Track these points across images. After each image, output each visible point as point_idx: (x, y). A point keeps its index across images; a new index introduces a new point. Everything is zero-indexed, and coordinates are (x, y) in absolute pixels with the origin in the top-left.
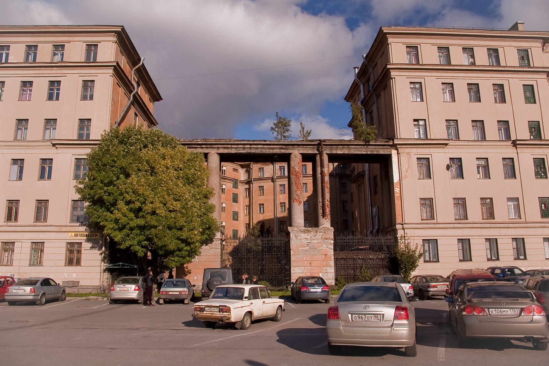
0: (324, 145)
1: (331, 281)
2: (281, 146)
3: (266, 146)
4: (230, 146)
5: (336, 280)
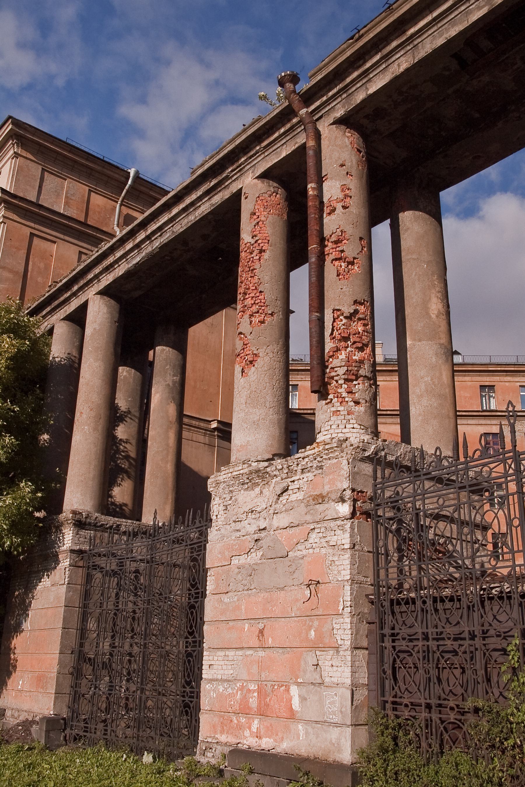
1: (334, 734)
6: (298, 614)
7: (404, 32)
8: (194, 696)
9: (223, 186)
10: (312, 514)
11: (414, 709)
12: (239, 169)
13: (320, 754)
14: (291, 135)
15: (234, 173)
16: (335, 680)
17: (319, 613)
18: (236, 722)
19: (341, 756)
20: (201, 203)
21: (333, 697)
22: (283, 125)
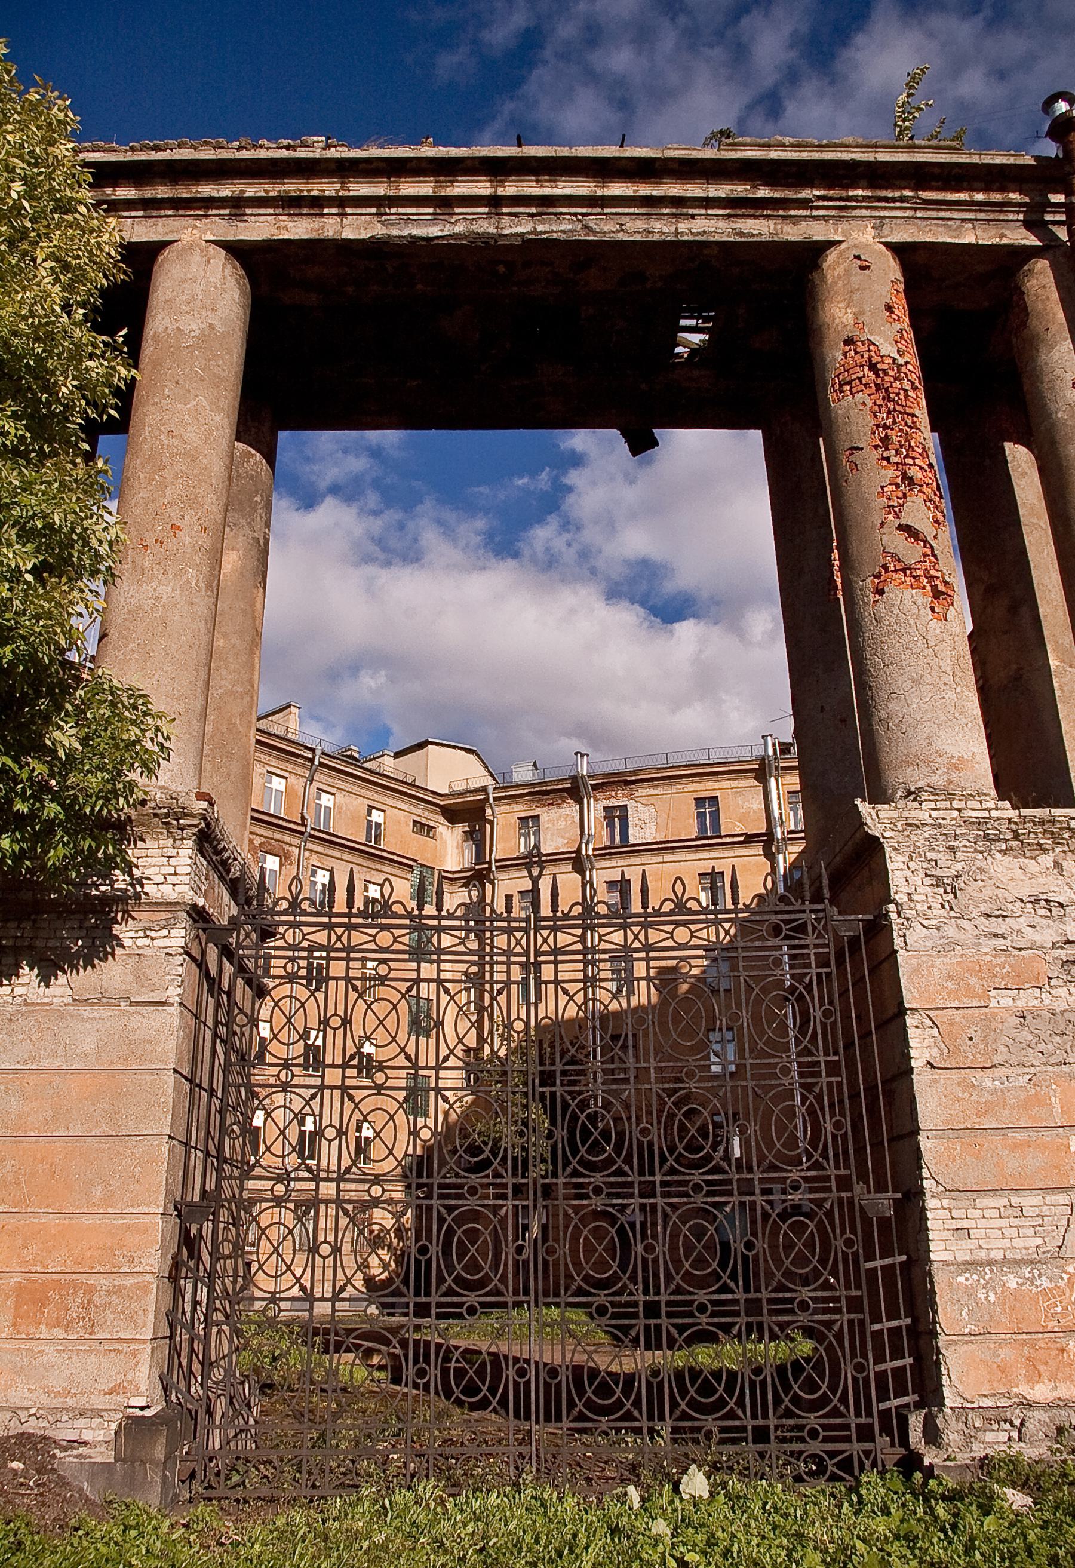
2: (741, 190)
3: (617, 189)
4: (330, 188)
9: (781, 213)
12: (843, 204)
14: (991, 216)
15: (826, 203)
20: (703, 212)
22: (986, 189)
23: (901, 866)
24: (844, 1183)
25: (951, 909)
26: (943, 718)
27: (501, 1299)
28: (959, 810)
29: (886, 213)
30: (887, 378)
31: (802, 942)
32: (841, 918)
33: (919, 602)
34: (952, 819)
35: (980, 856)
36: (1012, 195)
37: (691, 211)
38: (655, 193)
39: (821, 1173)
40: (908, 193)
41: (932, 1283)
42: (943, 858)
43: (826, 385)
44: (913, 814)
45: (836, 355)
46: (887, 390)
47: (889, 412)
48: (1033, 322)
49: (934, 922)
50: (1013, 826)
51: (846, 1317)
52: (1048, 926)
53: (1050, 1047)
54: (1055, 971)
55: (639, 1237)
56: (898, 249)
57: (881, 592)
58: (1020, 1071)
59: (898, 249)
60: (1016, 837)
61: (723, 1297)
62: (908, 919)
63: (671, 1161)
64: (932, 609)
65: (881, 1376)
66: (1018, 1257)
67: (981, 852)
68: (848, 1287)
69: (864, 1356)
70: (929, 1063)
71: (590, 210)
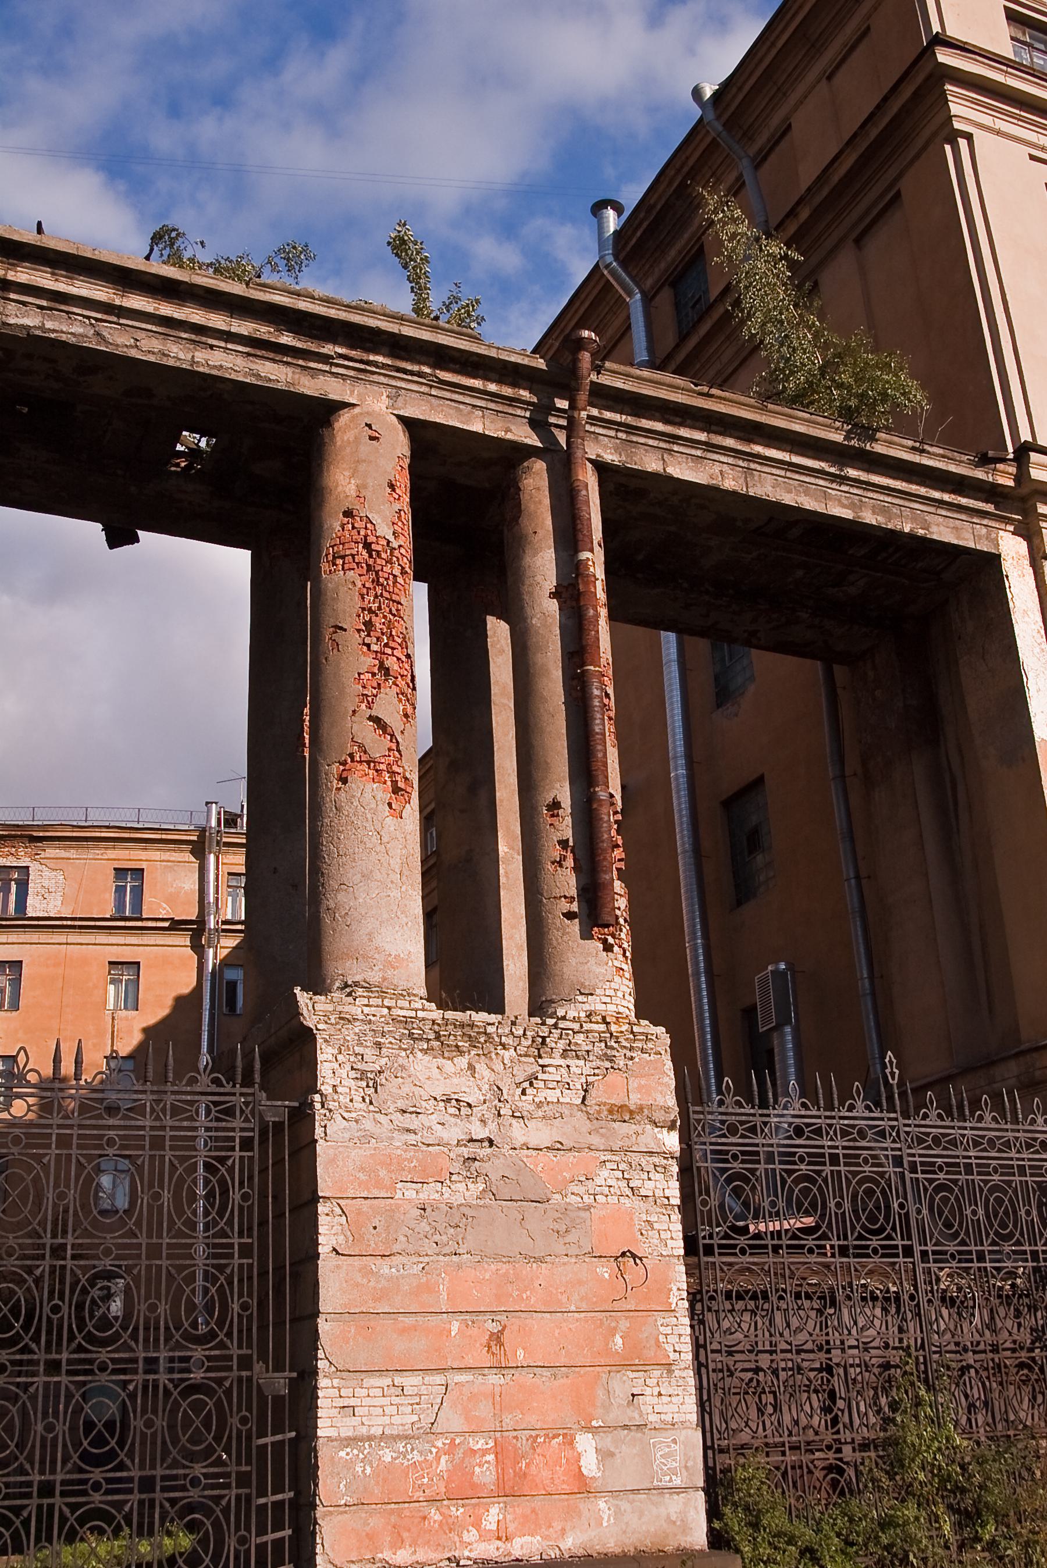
0: (605, 396)
1: (674, 1505)
2: (264, 331)
5: (717, 1487)
6: (584, 1306)
7: (750, 441)
8: (133, 1488)
9: (301, 362)
10: (602, 1135)
11: (743, 1454)
12: (362, 366)
13: (648, 1544)
14: (500, 408)
15: (346, 363)
16: (668, 1418)
17: (628, 1307)
18: (438, 1517)
19: (689, 1539)
20: (223, 344)
21: (669, 1447)
22: (499, 382)
23: (330, 1057)
24: (245, 1363)
25: (371, 1103)
26: (385, 916)
27: (763, 1242)
28: (389, 1008)
29: (403, 385)
30: (379, 561)
31: (229, 1125)
32: (269, 1103)
33: (378, 798)
34: (382, 1016)
35: (403, 1054)
36: (522, 392)
37: (211, 341)
38: (176, 315)
39: (225, 1352)
40: (427, 370)
41: (316, 1457)
42: (369, 1053)
43: (320, 552)
44: (347, 1008)
45: (334, 524)
46: (377, 573)
47: (376, 596)
48: (524, 521)
49: (354, 1115)
50: (436, 1027)
51: (234, 1491)
52: (456, 1124)
53: (444, 1238)
54: (456, 1167)
55: (39, 1415)
56: (409, 424)
57: (345, 781)
58: (415, 1259)
59: (409, 424)
60: (438, 1037)
61: (119, 1474)
62: (330, 1111)
63: (79, 1339)
64: (390, 805)
65: (261, 1548)
66: (395, 1432)
67: (405, 1050)
68: (239, 1463)
69: (248, 1529)
70: (334, 1249)
71: (105, 317)
